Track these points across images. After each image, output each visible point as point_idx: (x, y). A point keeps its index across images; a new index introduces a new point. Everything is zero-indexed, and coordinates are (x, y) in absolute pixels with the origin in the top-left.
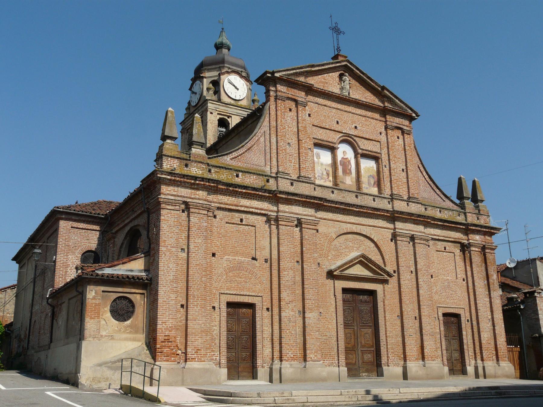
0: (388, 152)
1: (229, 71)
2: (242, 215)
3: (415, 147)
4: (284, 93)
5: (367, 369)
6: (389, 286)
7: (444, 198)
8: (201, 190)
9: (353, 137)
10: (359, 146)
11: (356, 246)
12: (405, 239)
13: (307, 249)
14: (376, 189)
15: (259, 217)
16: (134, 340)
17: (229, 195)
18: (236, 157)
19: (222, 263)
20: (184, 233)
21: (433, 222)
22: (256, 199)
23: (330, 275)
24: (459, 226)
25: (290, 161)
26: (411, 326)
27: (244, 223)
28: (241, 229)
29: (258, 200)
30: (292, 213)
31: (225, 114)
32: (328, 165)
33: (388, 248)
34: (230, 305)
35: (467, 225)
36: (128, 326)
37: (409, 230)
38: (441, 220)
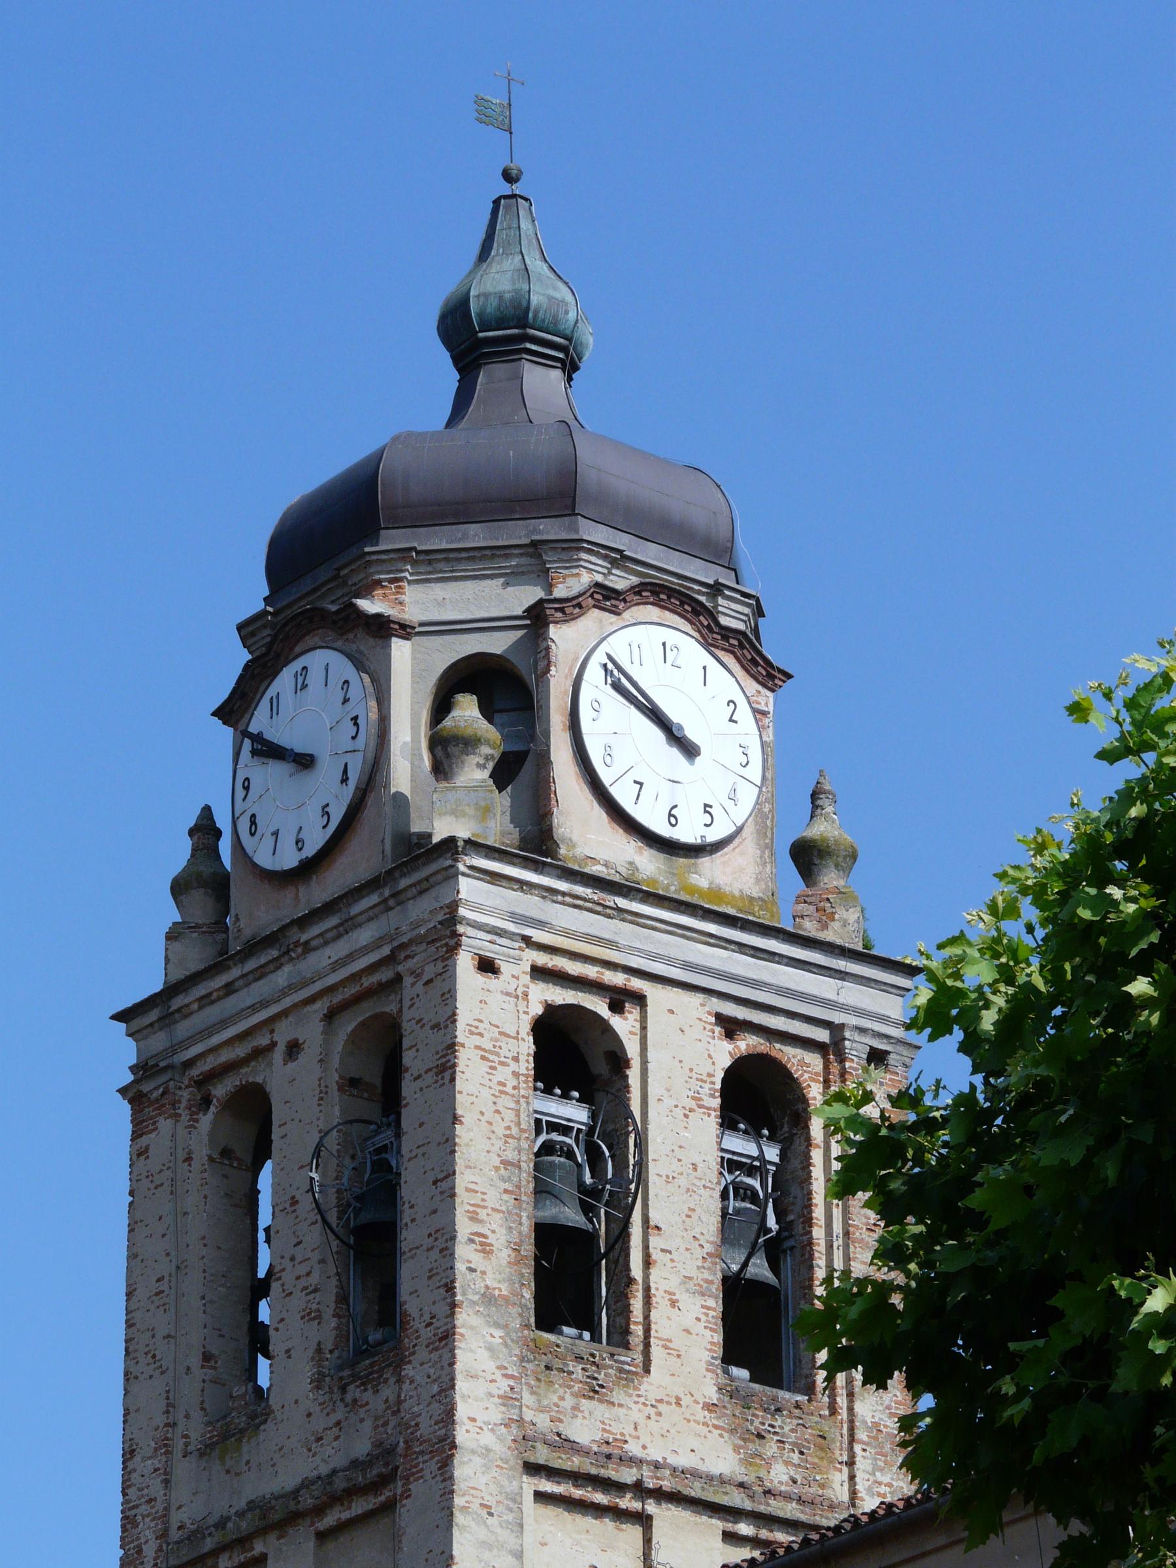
1: (621, 581)
3: (485, 253)
31: (591, 972)
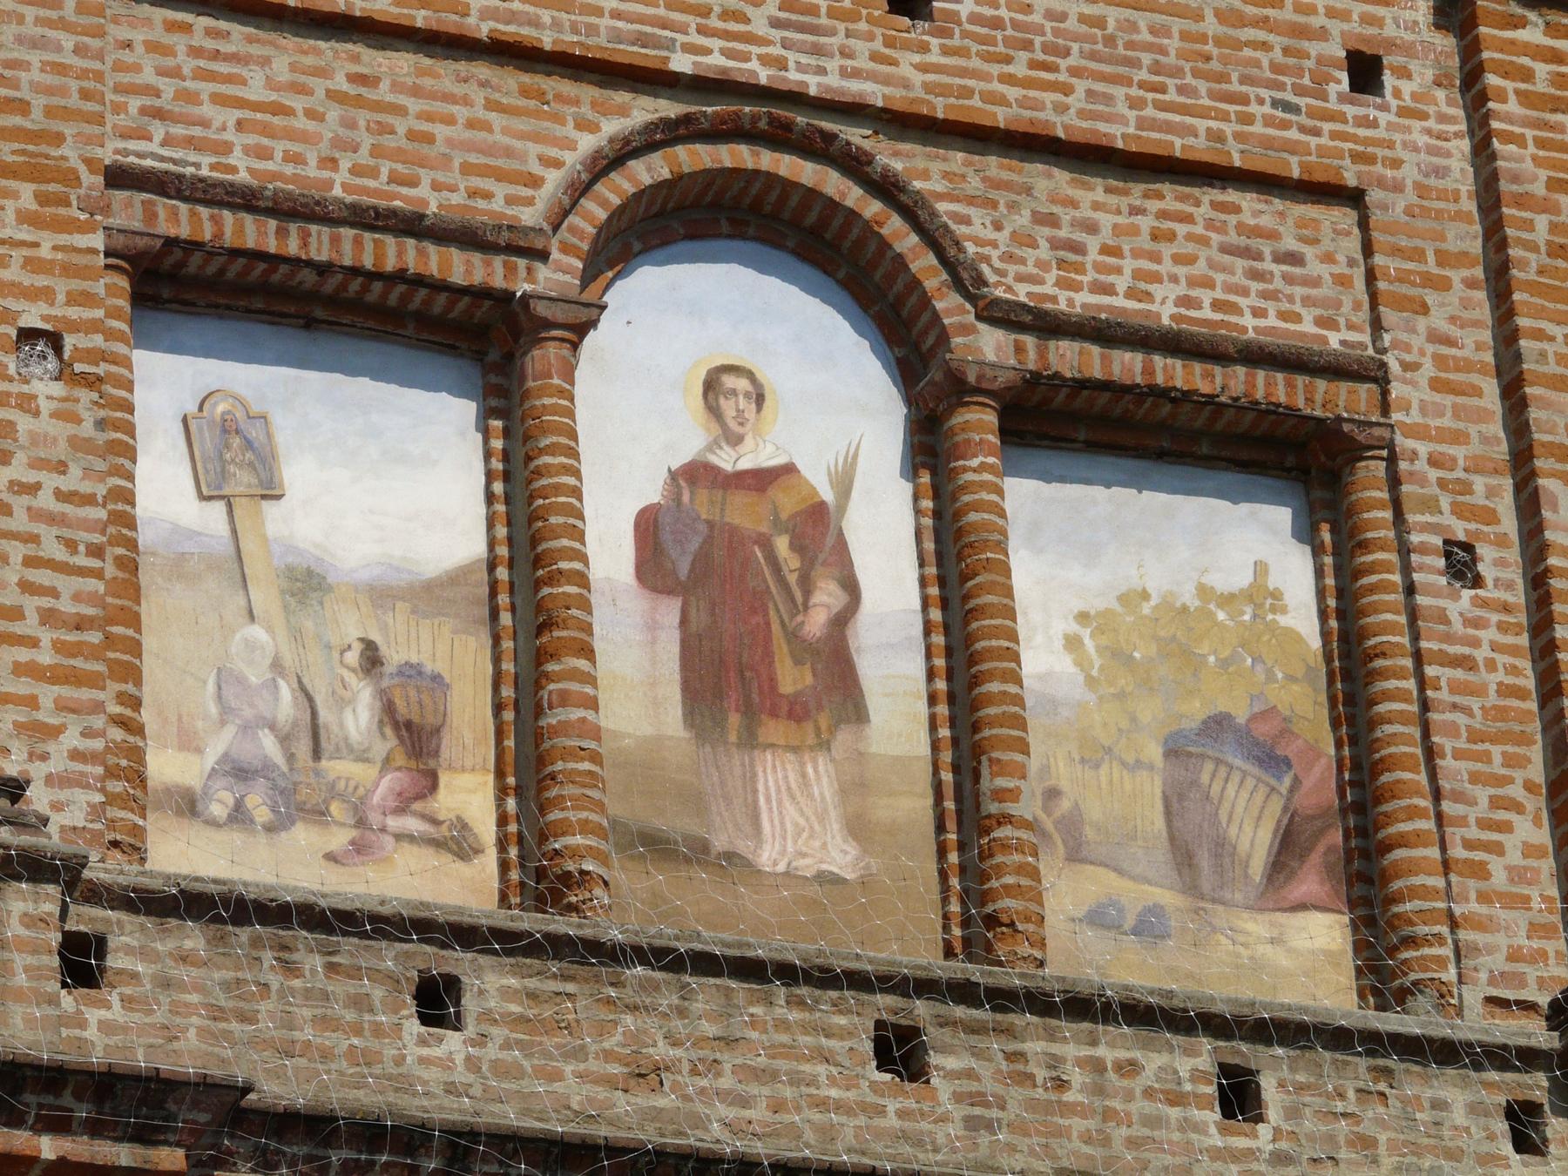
9: (855, 135)
14: (1323, 935)
32: (428, 596)
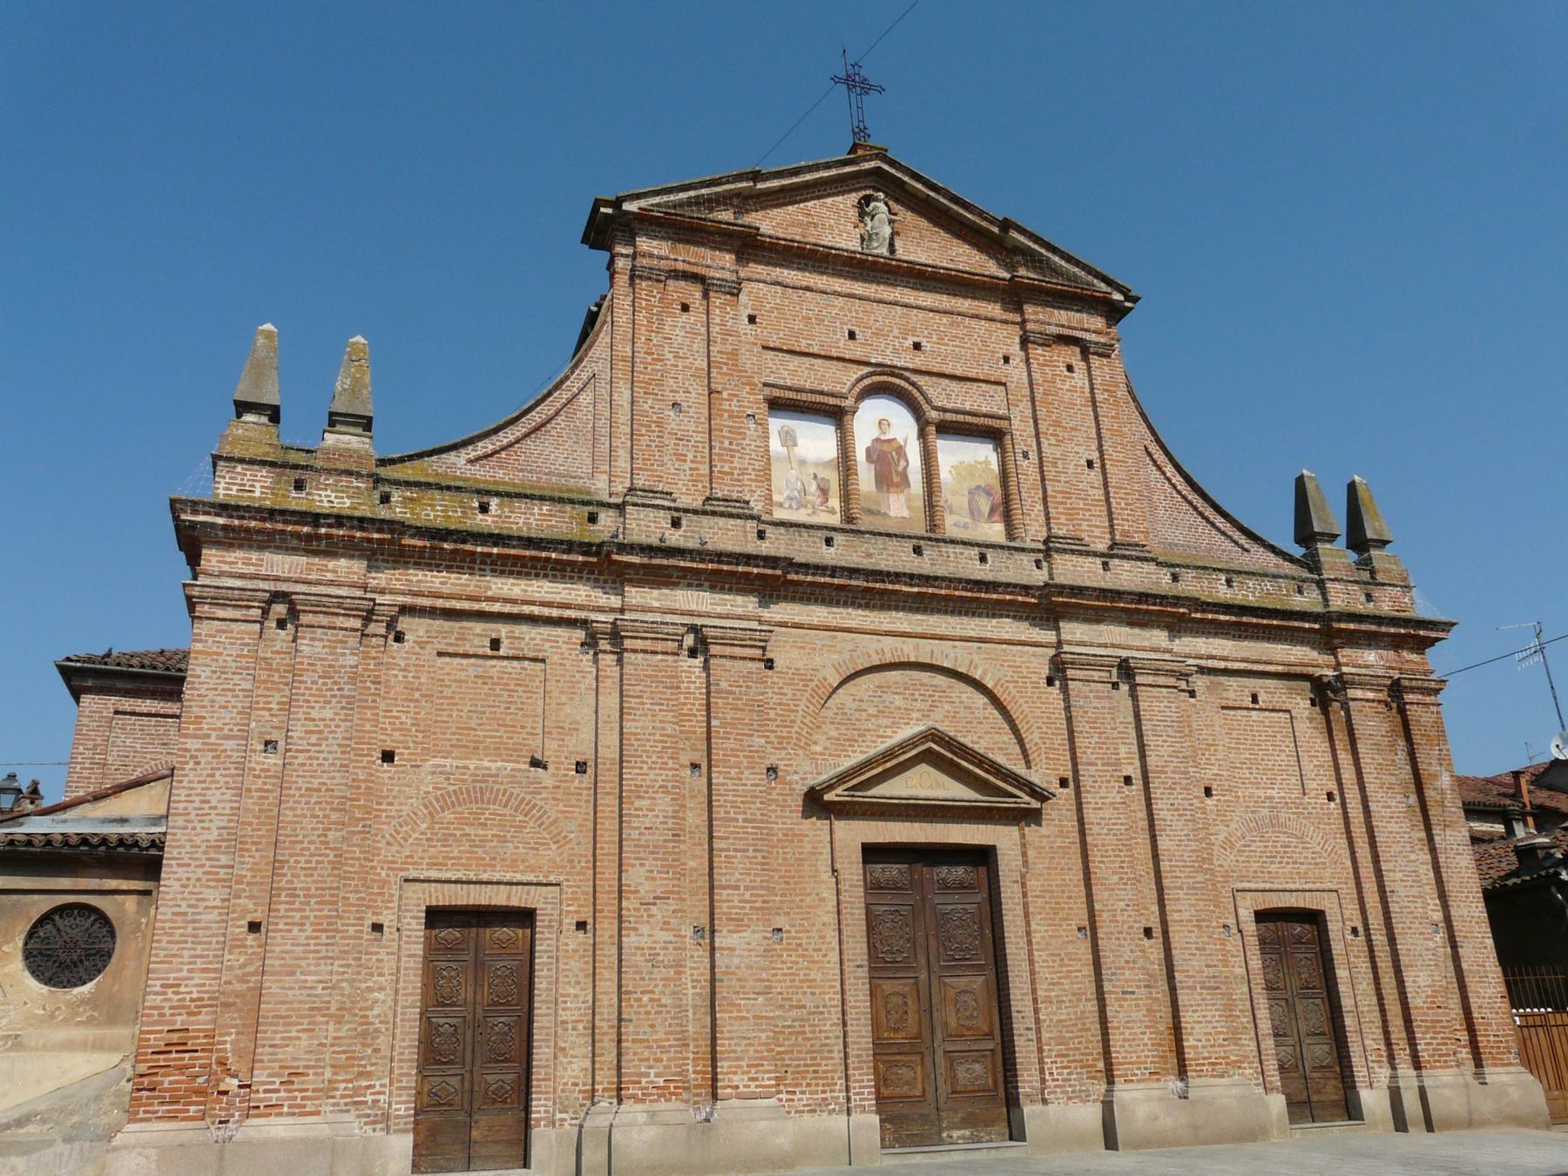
0: (1034, 411)
2: (500, 626)
3: (1130, 392)
4: (660, 258)
5: (970, 1114)
6: (1043, 830)
7: (1243, 540)
8: (343, 556)
9: (907, 374)
10: (928, 402)
11: (918, 705)
12: (1096, 675)
13: (723, 725)
15: (560, 631)
16: (98, 1046)
17: (449, 568)
18: (486, 456)
19: (412, 785)
20: (279, 690)
21: (1199, 615)
22: (546, 576)
23: (815, 803)
24: (1296, 624)
25: (681, 457)
26: (1131, 961)
27: (502, 652)
28: (494, 672)
29: (554, 579)
30: (672, 612)
32: (827, 464)
33: (1039, 707)
34: (436, 916)
35: (1325, 618)
36: (83, 1001)
37: (1113, 646)
38: (1227, 608)
